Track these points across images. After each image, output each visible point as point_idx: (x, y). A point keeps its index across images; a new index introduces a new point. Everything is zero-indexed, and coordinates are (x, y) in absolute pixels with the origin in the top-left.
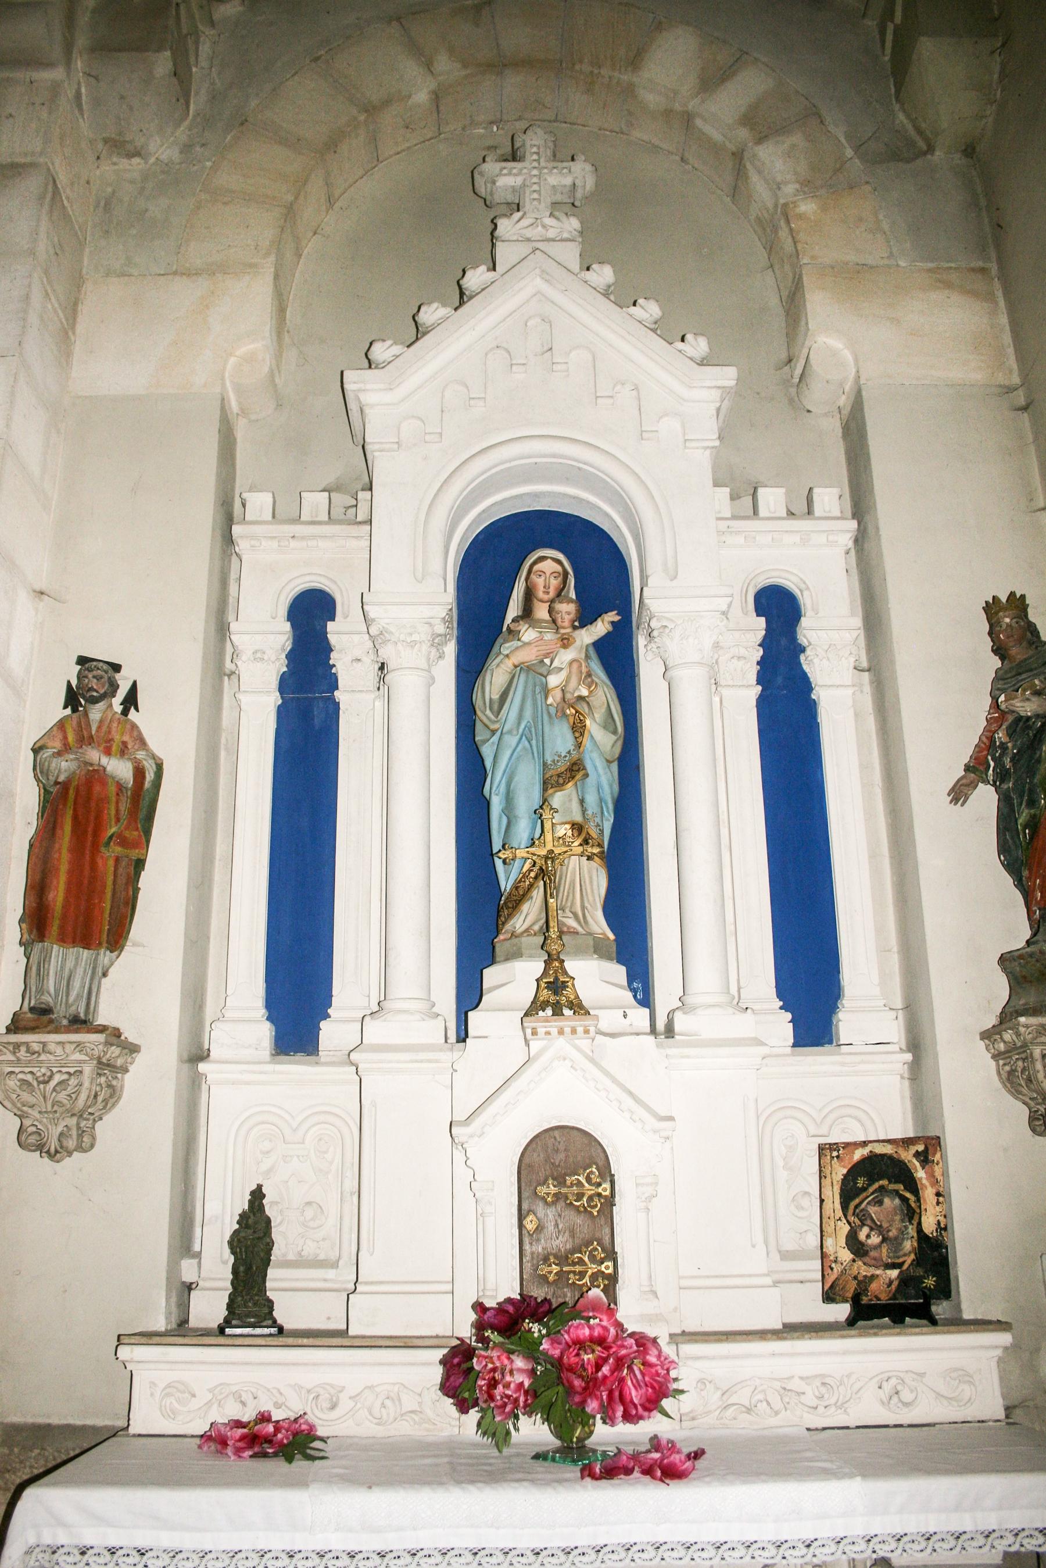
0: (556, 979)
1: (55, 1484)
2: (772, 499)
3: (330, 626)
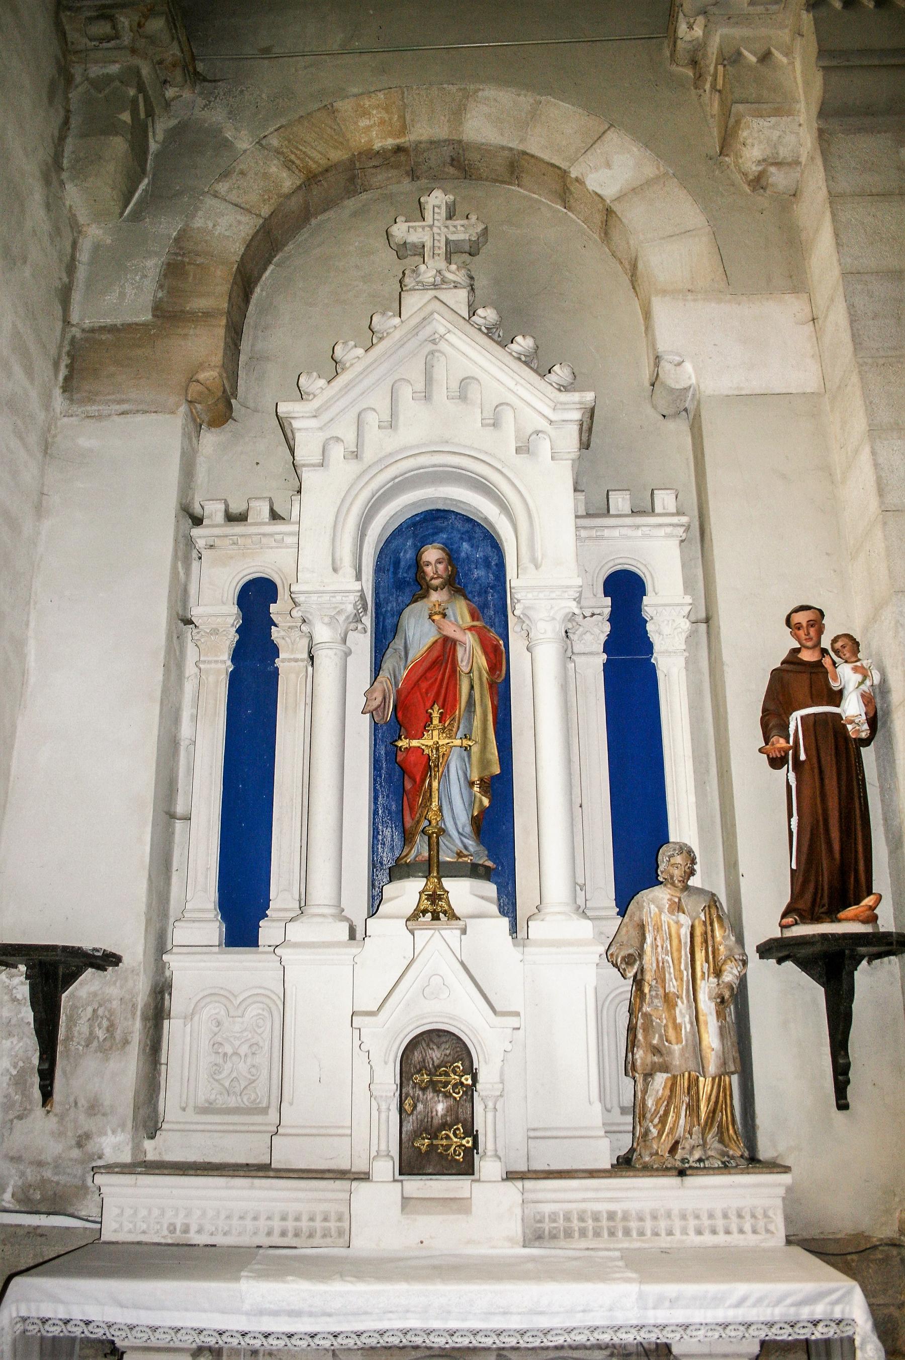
0: (435, 892)
1: (38, 1275)
2: (620, 502)
3: (273, 608)
